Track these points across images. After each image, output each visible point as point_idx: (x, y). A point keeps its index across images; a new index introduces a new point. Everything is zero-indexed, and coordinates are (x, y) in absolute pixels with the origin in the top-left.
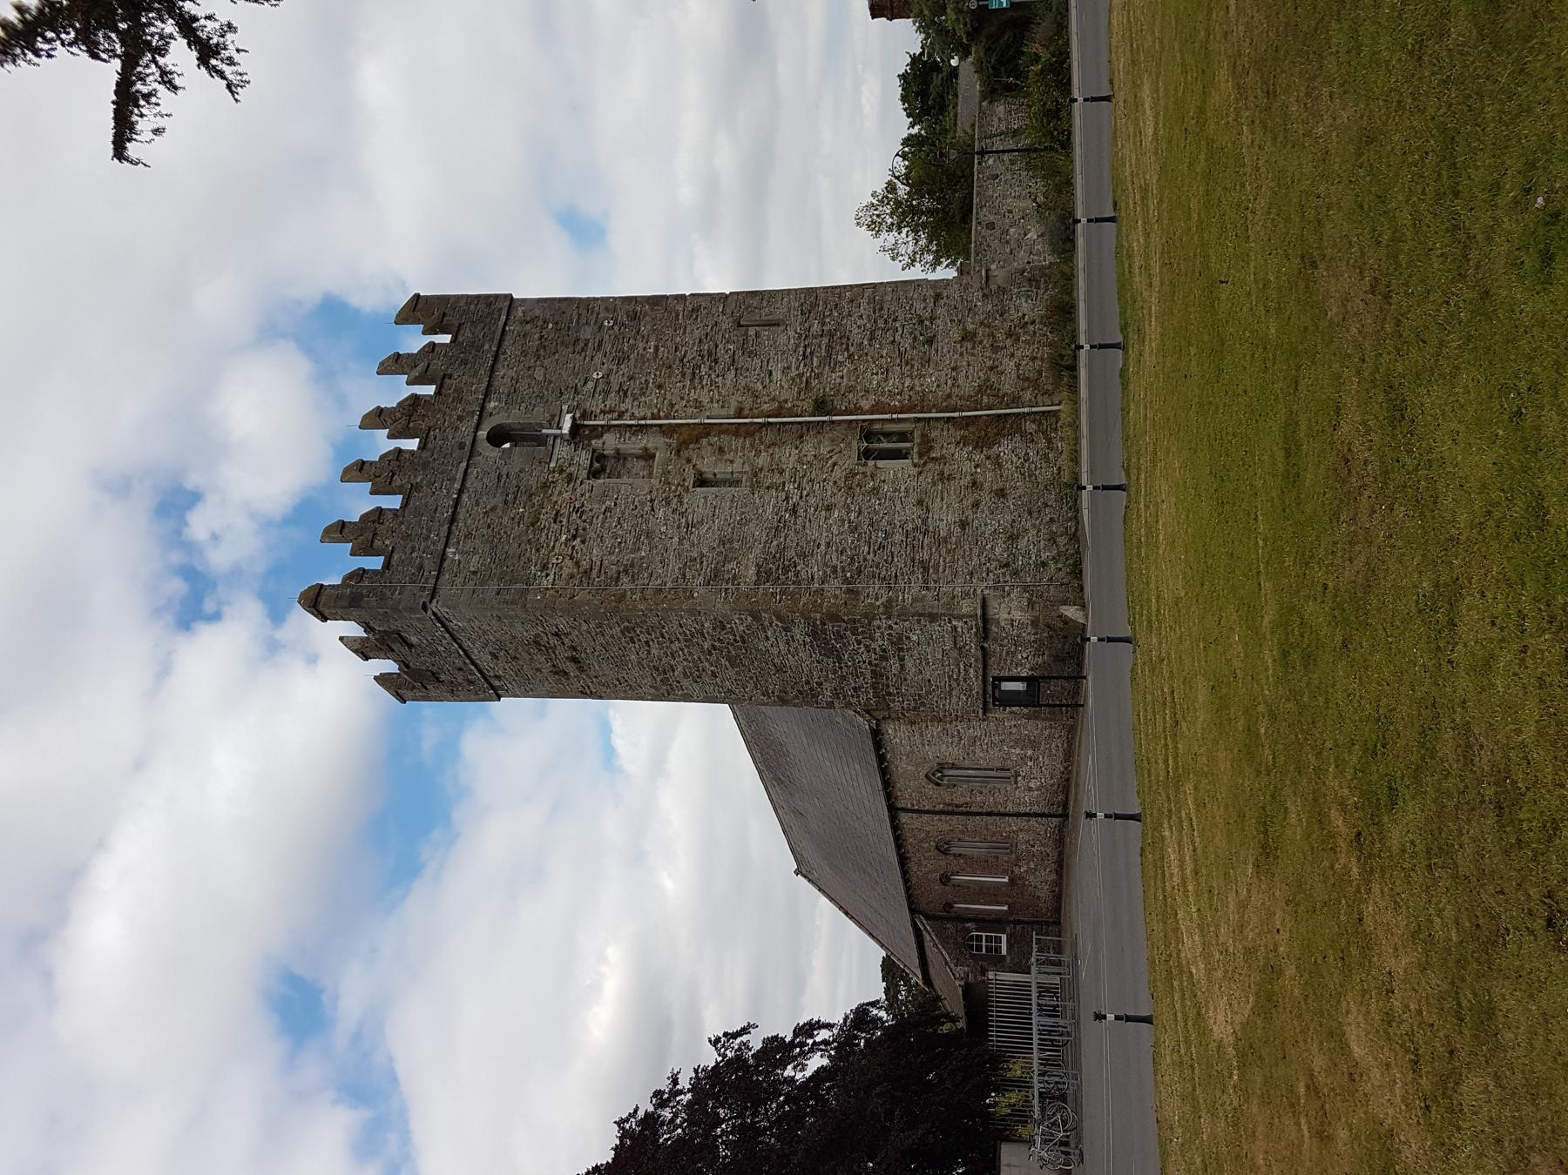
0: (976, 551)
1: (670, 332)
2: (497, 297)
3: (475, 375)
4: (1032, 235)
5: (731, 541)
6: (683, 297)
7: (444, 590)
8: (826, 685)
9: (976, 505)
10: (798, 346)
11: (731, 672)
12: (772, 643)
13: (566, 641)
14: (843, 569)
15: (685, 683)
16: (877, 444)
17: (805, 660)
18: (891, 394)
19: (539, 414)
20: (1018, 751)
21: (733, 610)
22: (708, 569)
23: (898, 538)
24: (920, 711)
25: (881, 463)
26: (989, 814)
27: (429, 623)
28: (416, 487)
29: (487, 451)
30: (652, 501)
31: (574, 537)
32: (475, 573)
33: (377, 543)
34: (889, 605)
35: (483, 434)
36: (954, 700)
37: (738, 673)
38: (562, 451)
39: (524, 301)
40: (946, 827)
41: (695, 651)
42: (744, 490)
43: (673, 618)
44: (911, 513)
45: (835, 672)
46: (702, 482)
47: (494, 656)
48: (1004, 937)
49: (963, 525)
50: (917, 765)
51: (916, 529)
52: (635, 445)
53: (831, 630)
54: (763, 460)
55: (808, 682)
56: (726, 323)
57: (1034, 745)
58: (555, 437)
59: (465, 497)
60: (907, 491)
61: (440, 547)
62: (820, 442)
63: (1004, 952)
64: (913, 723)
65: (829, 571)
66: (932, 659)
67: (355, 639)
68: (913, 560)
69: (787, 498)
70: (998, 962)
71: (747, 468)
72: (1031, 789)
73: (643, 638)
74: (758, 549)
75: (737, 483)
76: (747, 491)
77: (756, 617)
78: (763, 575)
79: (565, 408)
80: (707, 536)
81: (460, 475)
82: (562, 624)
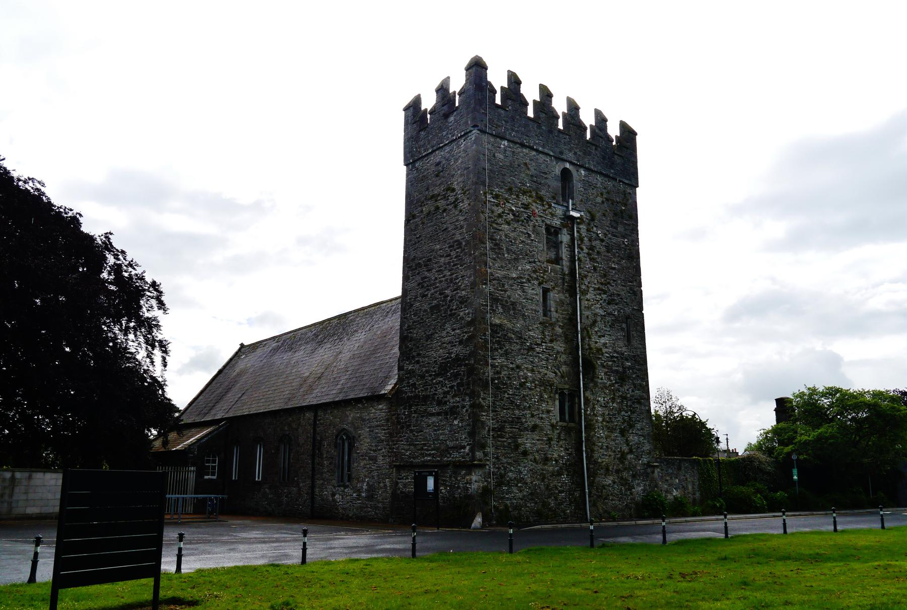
0: (510, 461)
1: (623, 277)
2: (637, 178)
3: (598, 163)
4: (675, 493)
5: (514, 309)
6: (641, 286)
7: (485, 138)
8: (417, 366)
9: (535, 461)
10: (617, 353)
11: (426, 307)
12: (449, 332)
13: (450, 207)
14: (499, 378)
15: (418, 278)
16: (569, 400)
17: (436, 353)
18: (593, 409)
19: (578, 197)
20: (365, 487)
21: (476, 309)
22: (498, 294)
23: (517, 412)
24: (397, 427)
25: (557, 403)
26: (313, 469)
27: (463, 127)
28: (539, 126)
29: (557, 170)
30: (535, 262)
31: (514, 215)
32: (494, 156)
33: (510, 102)
34: (480, 407)
35: (568, 166)
36: (406, 447)
37: (425, 311)
38: (559, 211)
39: (635, 194)
40: (301, 441)
41: (444, 285)
42: (542, 318)
43: (469, 272)
44: (531, 422)
45: (427, 372)
46: (546, 292)
47: (438, 164)
48: (215, 477)
49: (525, 453)
50: (352, 423)
51: (522, 424)
52: (564, 253)
53: (466, 372)
54: (559, 330)
55: (419, 355)
56: (628, 310)
57: (370, 497)
58: (568, 207)
59: (534, 153)
60: (542, 418)
61: (508, 137)
62: (568, 365)
63: (206, 477)
64: (388, 420)
65: (498, 369)
66: (440, 431)
67: (448, 85)
68: (505, 422)
69: (538, 344)
70: (200, 473)
71: (554, 320)
72: (342, 498)
73: (453, 253)
74: (509, 325)
75: (545, 315)
76: (541, 320)
77: (470, 324)
78: (496, 328)
79: (582, 213)
80: (516, 295)
81: (546, 151)
82: (464, 205)
